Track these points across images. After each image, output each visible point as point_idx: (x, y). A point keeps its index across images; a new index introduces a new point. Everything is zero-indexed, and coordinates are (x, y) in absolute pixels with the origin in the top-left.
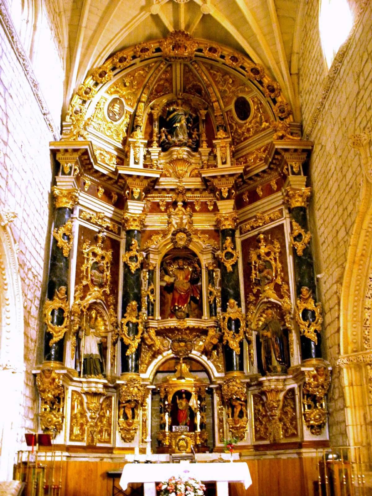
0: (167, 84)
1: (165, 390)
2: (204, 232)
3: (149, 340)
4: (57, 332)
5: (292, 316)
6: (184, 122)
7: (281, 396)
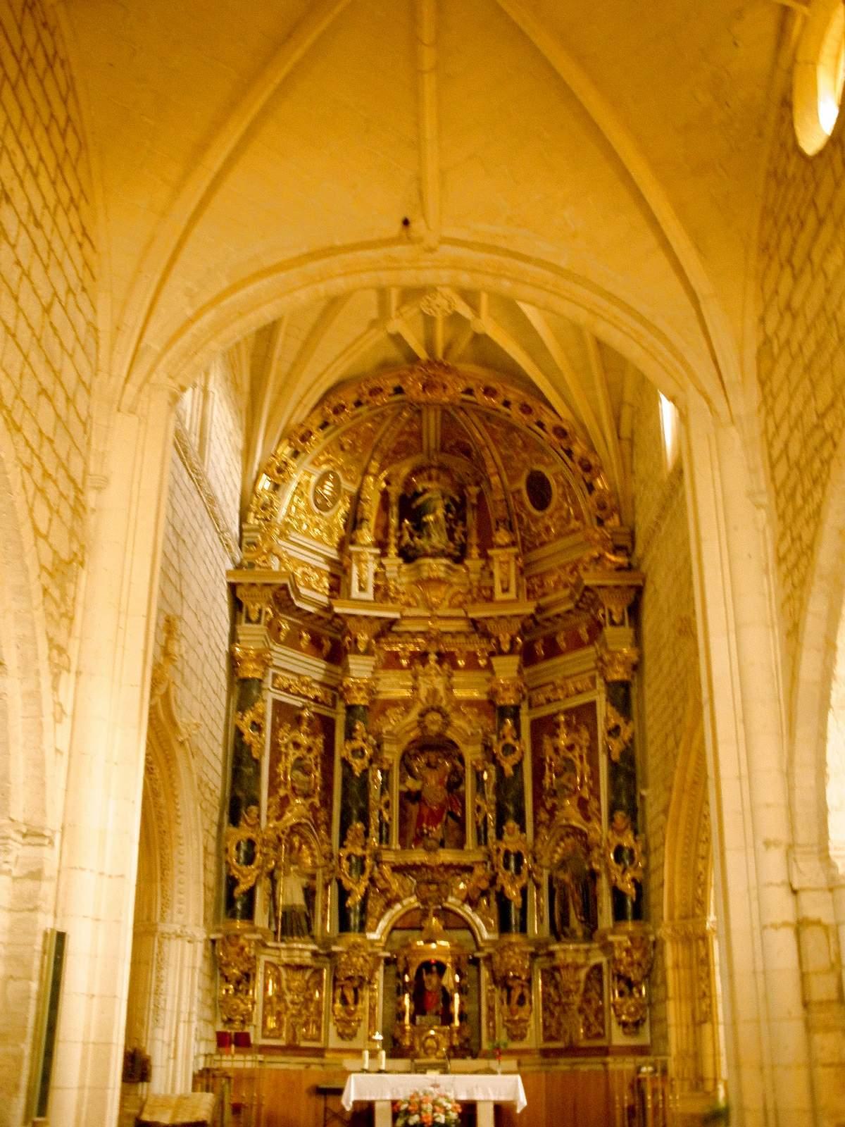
0: (412, 440)
1: (405, 958)
2: (471, 703)
3: (382, 882)
4: (245, 876)
5: (602, 851)
6: (440, 512)
7: (582, 974)
